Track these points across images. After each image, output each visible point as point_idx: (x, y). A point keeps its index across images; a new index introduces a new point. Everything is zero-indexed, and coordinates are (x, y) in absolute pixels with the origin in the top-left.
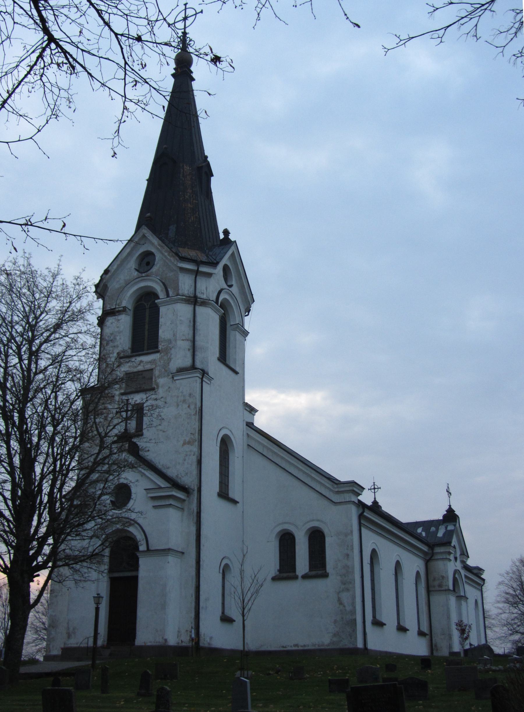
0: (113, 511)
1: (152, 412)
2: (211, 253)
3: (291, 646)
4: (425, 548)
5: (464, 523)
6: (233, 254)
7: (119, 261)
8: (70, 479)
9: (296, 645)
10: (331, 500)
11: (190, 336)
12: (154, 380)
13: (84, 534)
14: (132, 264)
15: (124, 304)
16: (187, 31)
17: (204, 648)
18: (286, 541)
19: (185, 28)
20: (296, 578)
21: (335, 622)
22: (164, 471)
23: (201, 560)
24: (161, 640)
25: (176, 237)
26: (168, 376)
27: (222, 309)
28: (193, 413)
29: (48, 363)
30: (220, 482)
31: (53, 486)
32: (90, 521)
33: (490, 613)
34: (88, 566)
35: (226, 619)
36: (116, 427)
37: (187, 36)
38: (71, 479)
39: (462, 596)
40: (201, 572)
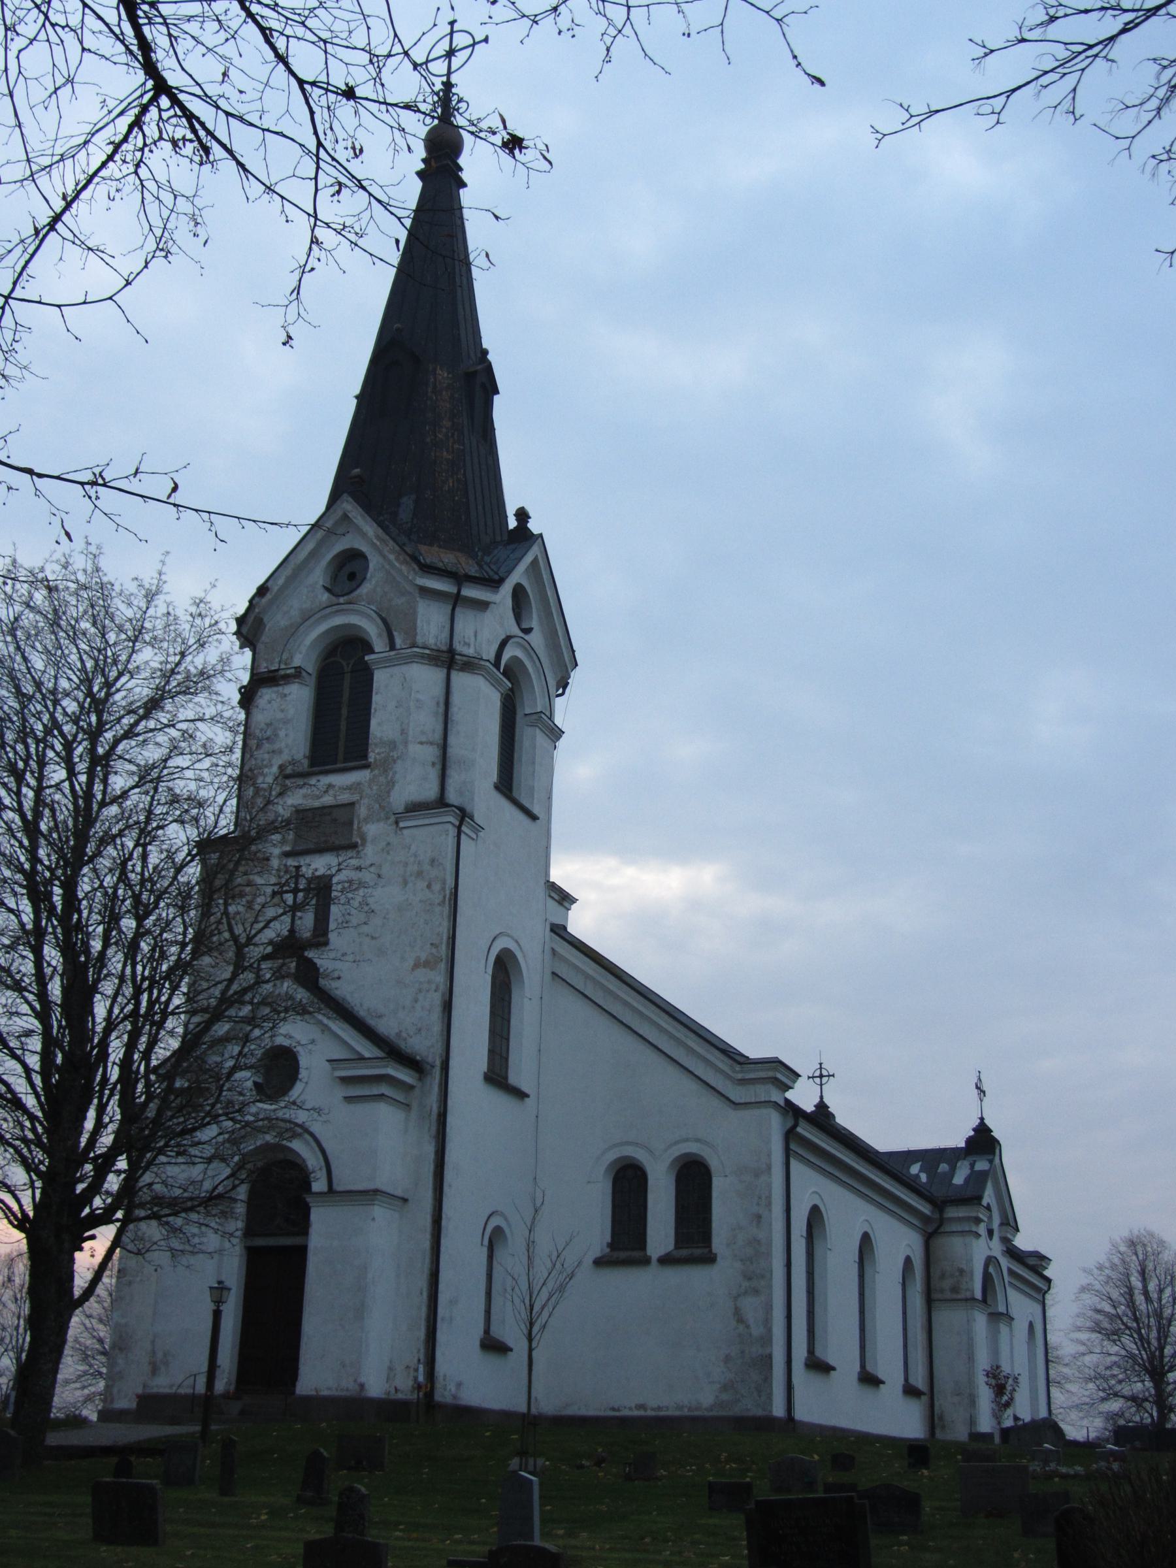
0: (260, 1105)
1: (350, 895)
2: (487, 559)
3: (630, 1409)
4: (925, 1208)
5: (1010, 1157)
6: (535, 562)
7: (291, 567)
9: (641, 1407)
11: (438, 736)
12: (355, 827)
13: (193, 1151)
14: (318, 575)
15: (297, 661)
17: (442, 1406)
18: (628, 1182)
19: (449, 73)
20: (645, 1261)
21: (727, 1359)
22: (372, 1022)
23: (444, 1216)
25: (415, 521)
26: (387, 818)
28: (437, 901)
29: (131, 782)
31: (130, 1047)
32: (209, 1123)
35: (493, 1346)
36: (272, 925)
37: (454, 90)
38: (171, 1033)
39: (1002, 1314)
40: (443, 1241)
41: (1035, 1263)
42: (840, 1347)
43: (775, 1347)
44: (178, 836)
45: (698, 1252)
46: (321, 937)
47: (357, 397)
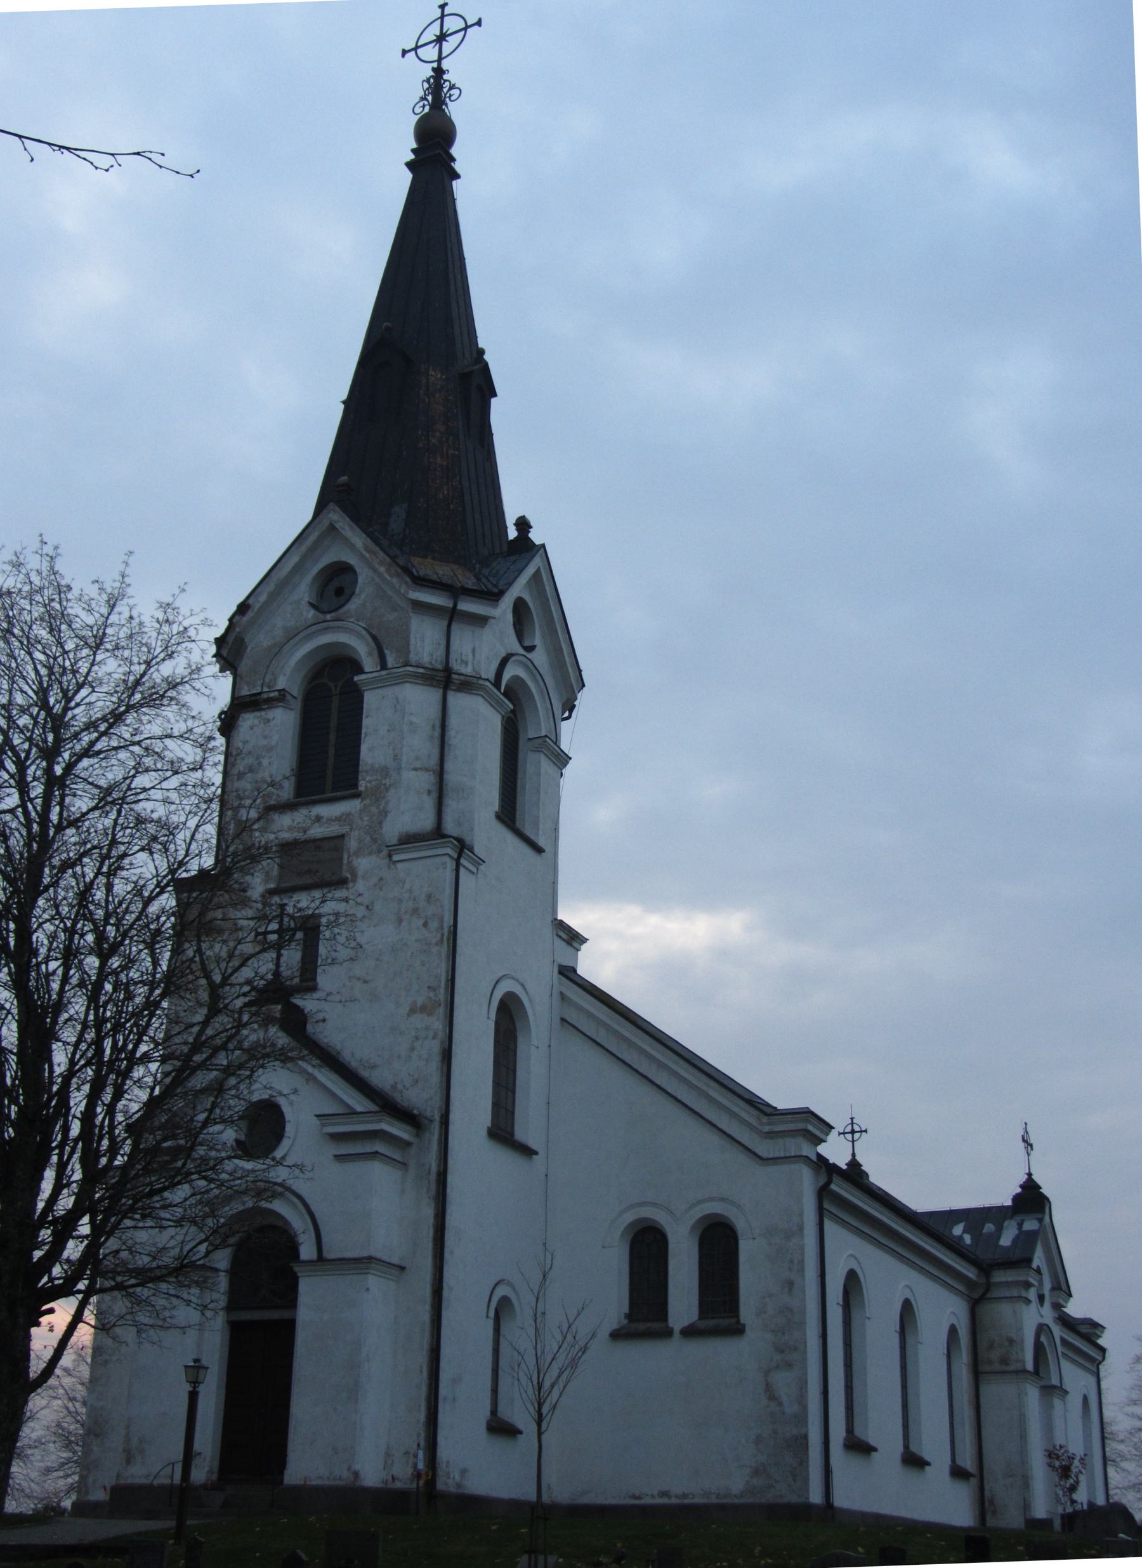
0: (237, 1161)
1: (336, 930)
2: (485, 571)
3: (653, 1496)
4: (971, 1273)
5: (1061, 1217)
6: (537, 574)
7: (275, 583)
8: (135, 1082)
9: (664, 1494)
10: (755, 1154)
12: (345, 862)
13: (164, 1214)
14: (304, 590)
15: (281, 684)
16: (445, 65)
17: (446, 1496)
18: (647, 1246)
19: (440, 59)
20: (667, 1333)
21: (758, 1440)
22: (365, 1073)
23: (445, 1285)
24: (346, 1474)
25: (407, 532)
26: (380, 851)
27: (510, 700)
28: (434, 941)
29: (92, 804)
30: (494, 1104)
31: (93, 1098)
32: (179, 1183)
33: (1114, 1428)
34: (172, 1292)
35: (500, 1428)
36: (250, 962)
37: (445, 77)
38: (139, 1082)
39: (1055, 1387)
40: (444, 1313)
41: (1086, 1332)
42: (882, 1426)
43: (810, 1426)
44: (145, 866)
45: (724, 1322)
46: (308, 981)
47: (344, 402)
